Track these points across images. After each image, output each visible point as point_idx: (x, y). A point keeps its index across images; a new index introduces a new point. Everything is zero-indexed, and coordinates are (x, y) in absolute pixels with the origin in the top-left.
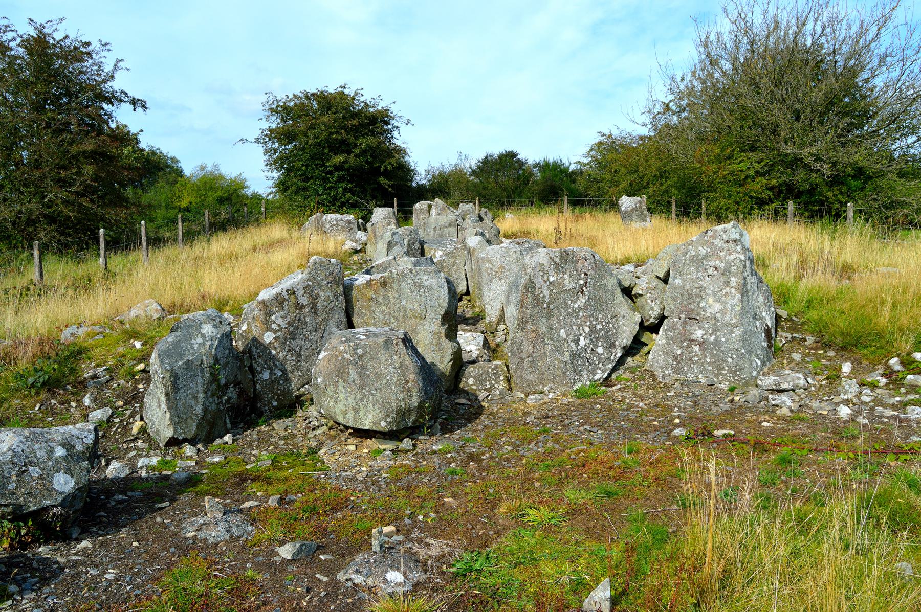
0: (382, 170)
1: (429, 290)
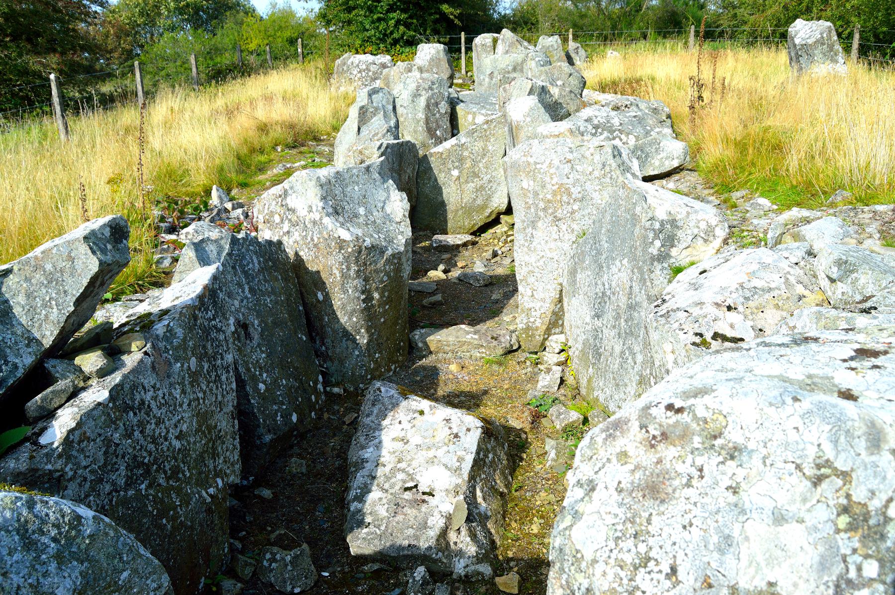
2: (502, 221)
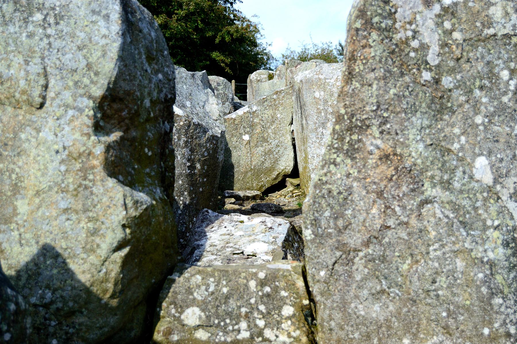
0: (217, 41)
1: (59, 18)
2: (288, 184)
